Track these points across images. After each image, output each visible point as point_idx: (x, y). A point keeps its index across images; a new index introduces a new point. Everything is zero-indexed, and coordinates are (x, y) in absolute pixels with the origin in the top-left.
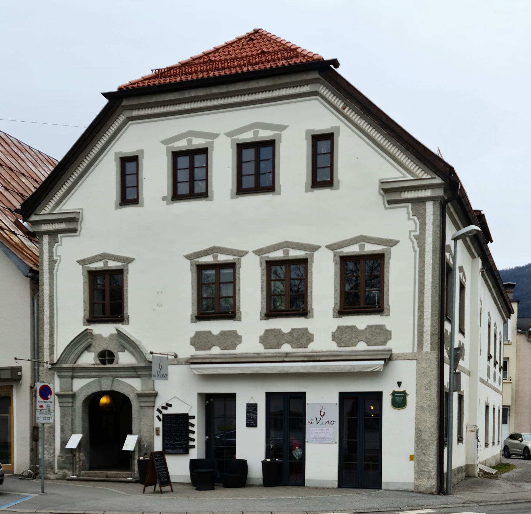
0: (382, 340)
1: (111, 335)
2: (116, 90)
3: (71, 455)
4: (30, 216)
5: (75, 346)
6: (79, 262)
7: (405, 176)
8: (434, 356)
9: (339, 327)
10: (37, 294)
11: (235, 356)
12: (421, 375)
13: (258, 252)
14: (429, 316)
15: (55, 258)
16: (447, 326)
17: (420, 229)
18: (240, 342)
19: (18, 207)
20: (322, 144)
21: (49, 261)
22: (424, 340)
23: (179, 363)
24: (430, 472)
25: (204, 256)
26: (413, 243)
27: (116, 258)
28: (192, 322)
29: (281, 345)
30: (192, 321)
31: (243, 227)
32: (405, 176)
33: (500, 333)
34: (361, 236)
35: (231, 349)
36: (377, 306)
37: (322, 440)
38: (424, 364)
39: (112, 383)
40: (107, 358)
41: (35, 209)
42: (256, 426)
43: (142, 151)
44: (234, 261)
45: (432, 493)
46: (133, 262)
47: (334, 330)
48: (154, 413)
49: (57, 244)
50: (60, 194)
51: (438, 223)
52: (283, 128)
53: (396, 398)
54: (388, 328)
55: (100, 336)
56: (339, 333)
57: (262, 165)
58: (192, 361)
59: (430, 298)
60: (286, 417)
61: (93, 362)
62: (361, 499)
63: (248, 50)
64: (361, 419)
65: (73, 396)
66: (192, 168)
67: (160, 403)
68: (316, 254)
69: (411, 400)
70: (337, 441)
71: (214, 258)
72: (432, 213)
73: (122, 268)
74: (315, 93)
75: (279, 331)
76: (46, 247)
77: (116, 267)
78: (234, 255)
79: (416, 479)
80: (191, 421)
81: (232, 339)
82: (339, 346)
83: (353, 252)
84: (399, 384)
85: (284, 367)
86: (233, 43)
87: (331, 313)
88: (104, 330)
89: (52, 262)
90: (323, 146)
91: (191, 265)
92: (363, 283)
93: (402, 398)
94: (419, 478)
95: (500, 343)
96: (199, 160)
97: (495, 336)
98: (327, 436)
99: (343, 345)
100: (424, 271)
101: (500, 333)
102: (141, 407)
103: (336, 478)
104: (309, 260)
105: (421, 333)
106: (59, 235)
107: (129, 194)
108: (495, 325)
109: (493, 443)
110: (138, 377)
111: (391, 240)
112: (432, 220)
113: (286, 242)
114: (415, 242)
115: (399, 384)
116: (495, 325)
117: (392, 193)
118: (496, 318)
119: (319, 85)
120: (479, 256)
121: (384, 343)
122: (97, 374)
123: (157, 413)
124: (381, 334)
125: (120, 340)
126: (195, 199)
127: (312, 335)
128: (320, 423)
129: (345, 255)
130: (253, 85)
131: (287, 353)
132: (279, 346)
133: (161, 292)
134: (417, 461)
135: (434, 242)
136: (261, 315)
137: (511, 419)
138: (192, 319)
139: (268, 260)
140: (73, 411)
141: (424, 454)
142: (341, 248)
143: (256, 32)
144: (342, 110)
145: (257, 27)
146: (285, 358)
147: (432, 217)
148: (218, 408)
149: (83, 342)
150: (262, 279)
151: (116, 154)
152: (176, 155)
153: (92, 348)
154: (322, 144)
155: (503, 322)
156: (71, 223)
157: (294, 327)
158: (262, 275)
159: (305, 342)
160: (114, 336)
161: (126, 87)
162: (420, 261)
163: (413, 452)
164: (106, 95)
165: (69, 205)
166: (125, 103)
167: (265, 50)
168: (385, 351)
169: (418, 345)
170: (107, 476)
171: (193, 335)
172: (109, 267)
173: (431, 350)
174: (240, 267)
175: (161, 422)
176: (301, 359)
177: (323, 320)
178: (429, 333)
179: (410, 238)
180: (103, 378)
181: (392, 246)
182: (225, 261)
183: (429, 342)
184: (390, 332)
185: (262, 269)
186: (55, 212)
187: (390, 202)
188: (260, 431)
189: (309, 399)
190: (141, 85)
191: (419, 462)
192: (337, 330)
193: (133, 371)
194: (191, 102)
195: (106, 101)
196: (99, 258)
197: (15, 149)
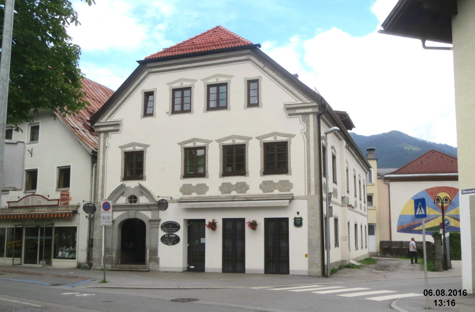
1: (136, 187)
2: (143, 59)
4: (94, 123)
6: (119, 147)
7: (297, 101)
8: (317, 198)
9: (263, 181)
10: (95, 164)
12: (310, 208)
13: (218, 141)
14: (314, 175)
15: (107, 145)
16: (324, 180)
18: (208, 190)
19: (88, 119)
20: (252, 85)
21: (104, 147)
23: (173, 202)
24: (317, 264)
26: (303, 136)
27: (140, 145)
30: (181, 179)
31: (211, 129)
32: (297, 101)
33: (364, 180)
43: (156, 89)
45: (319, 277)
50: (111, 112)
51: (316, 125)
52: (231, 77)
54: (291, 182)
55: (129, 188)
57: (221, 95)
58: (180, 201)
60: (234, 234)
61: (125, 202)
63: (213, 37)
64: (277, 234)
66: (182, 97)
69: (305, 222)
75: (230, 184)
76: (102, 139)
79: (309, 268)
82: (264, 192)
84: (298, 213)
86: (205, 33)
88: (132, 184)
89: (105, 147)
90: (253, 86)
92: (276, 157)
95: (364, 186)
96: (186, 93)
97: (360, 182)
101: (364, 180)
105: (309, 185)
106: (110, 133)
107: (147, 112)
108: (359, 175)
109: (362, 247)
110: (150, 210)
114: (304, 135)
115: (298, 213)
116: (359, 175)
117: (291, 110)
118: (360, 171)
120: (344, 139)
121: (289, 190)
124: (287, 185)
132: (230, 192)
135: (314, 136)
137: (377, 231)
143: (217, 27)
145: (218, 25)
146: (233, 199)
149: (120, 191)
152: (174, 90)
153: (125, 194)
154: (252, 85)
155: (365, 173)
156: (116, 127)
158: (220, 153)
161: (149, 57)
162: (307, 146)
163: (307, 253)
164: (138, 62)
165: (116, 117)
166: (148, 65)
167: (222, 37)
169: (308, 192)
170: (131, 268)
171: (181, 186)
176: (243, 199)
185: (220, 150)
190: (157, 57)
193: (147, 207)
195: (138, 64)
197: (90, 90)
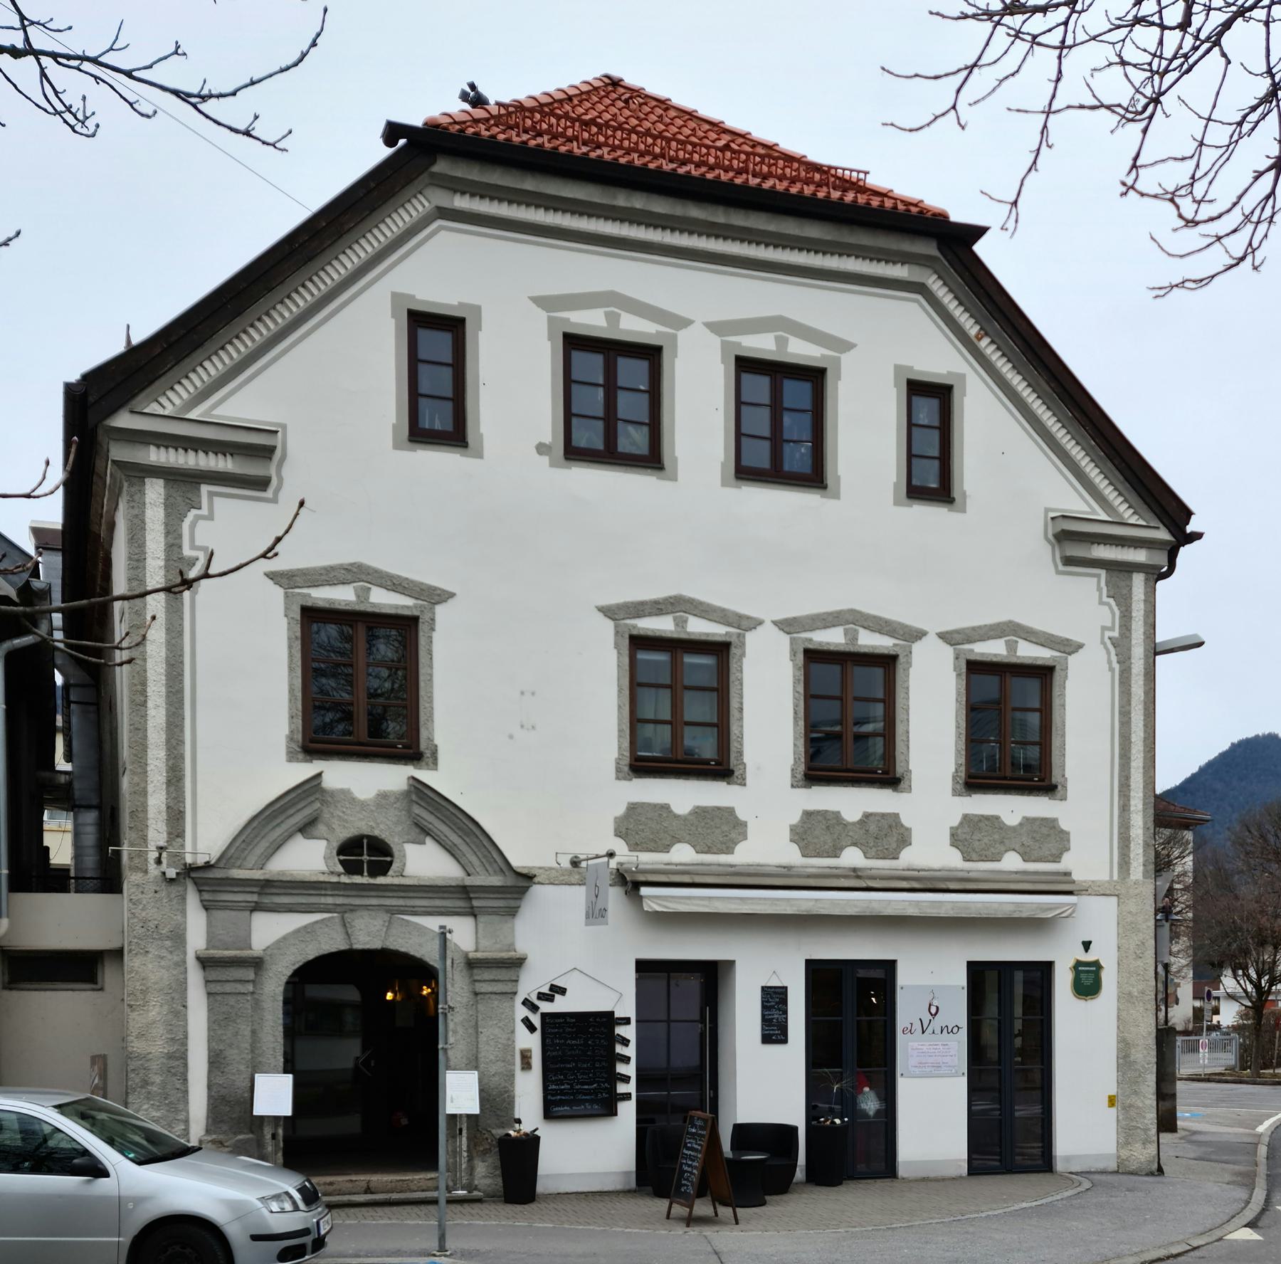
0: (1054, 851)
1: (383, 796)
3: (251, 1136)
5: (275, 817)
7: (1094, 512)
9: (965, 817)
11: (734, 870)
12: (1125, 927)
14: (1140, 807)
17: (1120, 626)
22: (1132, 856)
25: (650, 615)
28: (618, 778)
29: (842, 849)
30: (620, 775)
34: (1010, 622)
35: (721, 852)
36: (1036, 776)
37: (934, 1071)
38: (1132, 906)
39: (388, 928)
40: (365, 858)
41: (134, 396)
42: (785, 1041)
44: (728, 639)
46: (450, 601)
47: (956, 823)
48: (513, 1012)
49: (194, 512)
53: (1083, 976)
54: (1064, 825)
55: (346, 793)
56: (967, 829)
57: (787, 419)
59: (1141, 770)
60: (850, 1018)
62: (1017, 1193)
64: (1011, 1021)
65: (257, 964)
67: (530, 984)
68: (917, 647)
69: (1109, 978)
70: (964, 1068)
71: (677, 625)
72: (1143, 597)
73: (416, 613)
74: (920, 288)
77: (397, 607)
78: (729, 625)
80: (620, 1030)
81: (725, 828)
83: (995, 655)
84: (1087, 945)
85: (1001, 903)
87: (948, 784)
88: (364, 782)
91: (617, 633)
93: (1092, 976)
94: (1127, 1143)
98: (947, 1059)
99: (974, 856)
100: (1129, 713)
102: (476, 994)
103: (964, 1154)
104: (902, 659)
106: (205, 489)
110: (473, 913)
111: (1068, 640)
112: (1142, 612)
113: (852, 611)
115: (1087, 945)
119: (929, 271)
121: (1056, 858)
122: (340, 901)
123: (522, 1012)
124: (1049, 838)
125: (417, 810)
126: (437, 447)
127: (909, 830)
128: (930, 1030)
129: (979, 658)
130: (790, 227)
131: (855, 870)
132: (835, 853)
133: (533, 694)
134: (1124, 1108)
136: (793, 776)
138: (618, 770)
139: (811, 647)
140: (257, 1005)
141: (1136, 1093)
142: (970, 642)
144: (975, 341)
146: (858, 881)
147: (1142, 606)
148: (686, 994)
149: (296, 810)
150: (795, 691)
151: (962, 377)
153: (321, 828)
156: (251, 460)
157: (870, 810)
159: (894, 845)
160: (392, 799)
162: (1121, 693)
166: (442, 166)
168: (1058, 873)
169: (1121, 866)
170: (368, 1190)
171: (621, 810)
172: (374, 605)
173: (1145, 876)
174: (743, 655)
175: (538, 1034)
177: (931, 800)
178: (1141, 842)
179: (1103, 643)
180: (358, 913)
181: (1070, 654)
182: (708, 634)
183: (1141, 860)
184: (1068, 833)
186: (193, 415)
187: (1069, 561)
188: (792, 1056)
189: (903, 978)
191: (1126, 1108)
192: (961, 823)
193: (462, 898)
194: (622, 221)
196: (342, 575)
